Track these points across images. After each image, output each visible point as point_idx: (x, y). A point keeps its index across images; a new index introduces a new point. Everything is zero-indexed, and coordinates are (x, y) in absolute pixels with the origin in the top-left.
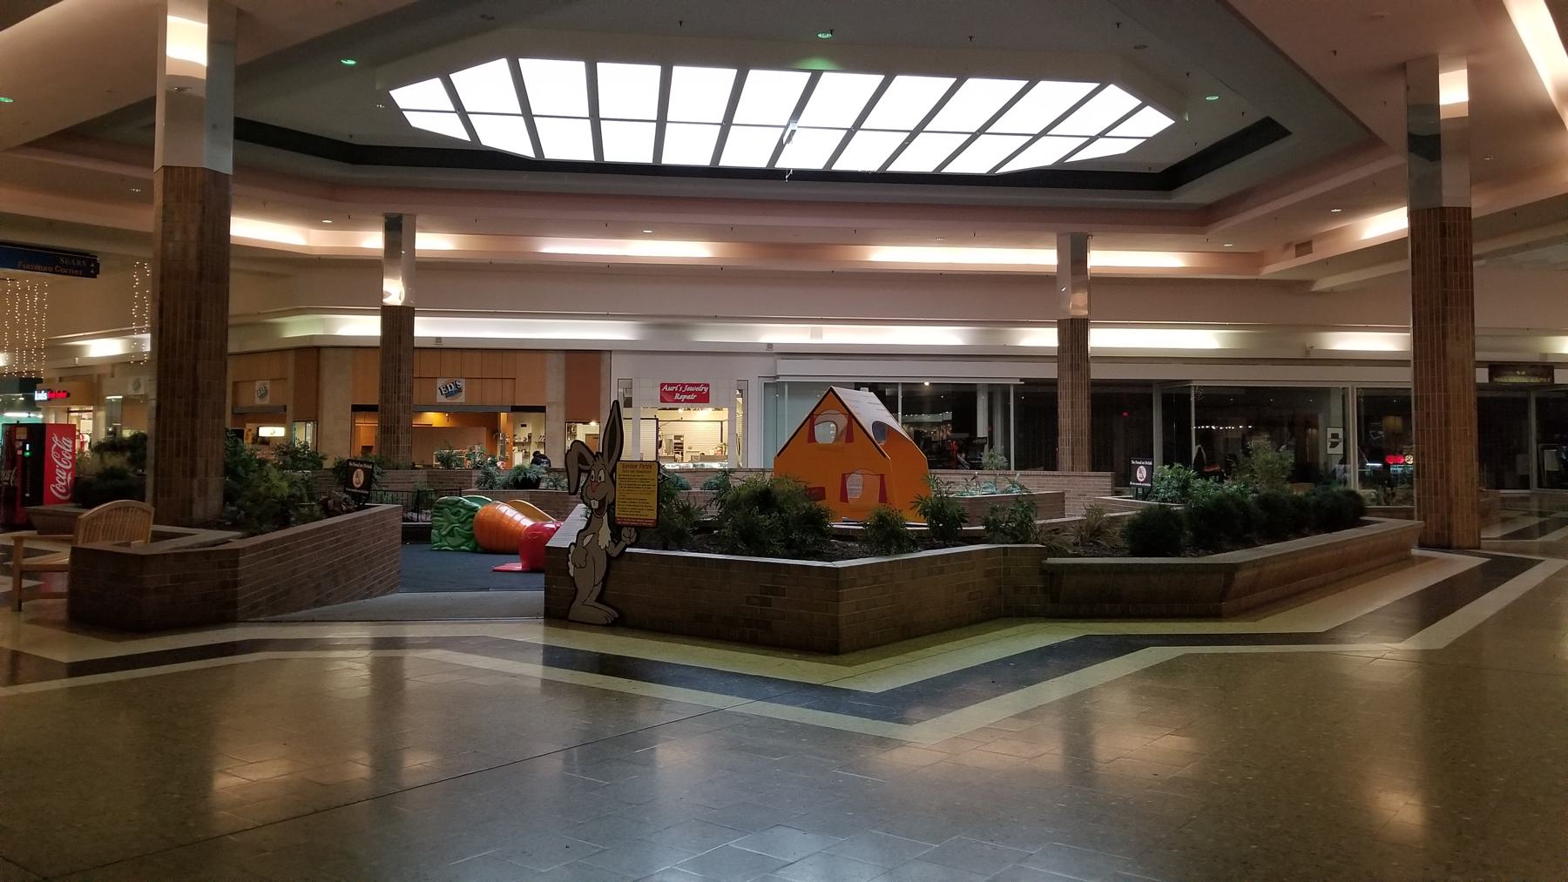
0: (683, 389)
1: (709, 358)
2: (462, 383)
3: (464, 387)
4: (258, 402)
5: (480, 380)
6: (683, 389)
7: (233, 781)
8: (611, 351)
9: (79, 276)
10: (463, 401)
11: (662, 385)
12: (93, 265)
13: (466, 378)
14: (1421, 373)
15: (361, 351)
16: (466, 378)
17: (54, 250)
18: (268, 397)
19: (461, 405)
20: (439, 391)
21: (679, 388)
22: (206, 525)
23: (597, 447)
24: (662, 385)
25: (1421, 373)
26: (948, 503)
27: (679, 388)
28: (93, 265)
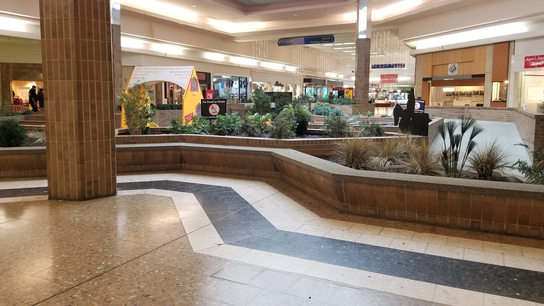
0: (537, 59)
1: (468, 50)
2: (457, 66)
3: (457, 67)
4: (450, 73)
5: (470, 62)
6: (537, 59)
7: (532, 203)
8: (515, 41)
9: (328, 42)
10: (457, 74)
11: (526, 58)
12: (332, 38)
13: (458, 63)
14: (103, 45)
15: (451, 52)
16: (458, 63)
17: (308, 37)
18: (456, 71)
19: (456, 76)
20: (449, 69)
21: (534, 59)
22: (69, 184)
23: (404, 108)
24: (526, 58)
25: (103, 45)
26: (523, 167)
27: (534, 59)
28: (332, 38)
